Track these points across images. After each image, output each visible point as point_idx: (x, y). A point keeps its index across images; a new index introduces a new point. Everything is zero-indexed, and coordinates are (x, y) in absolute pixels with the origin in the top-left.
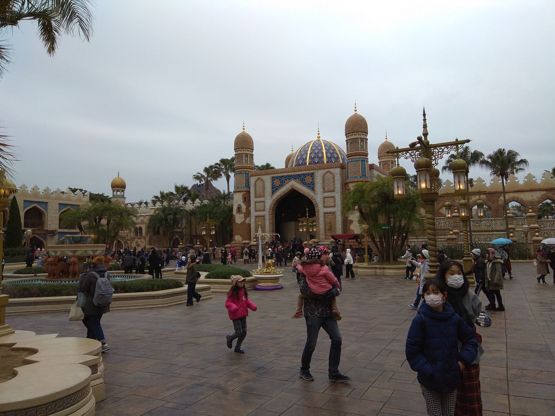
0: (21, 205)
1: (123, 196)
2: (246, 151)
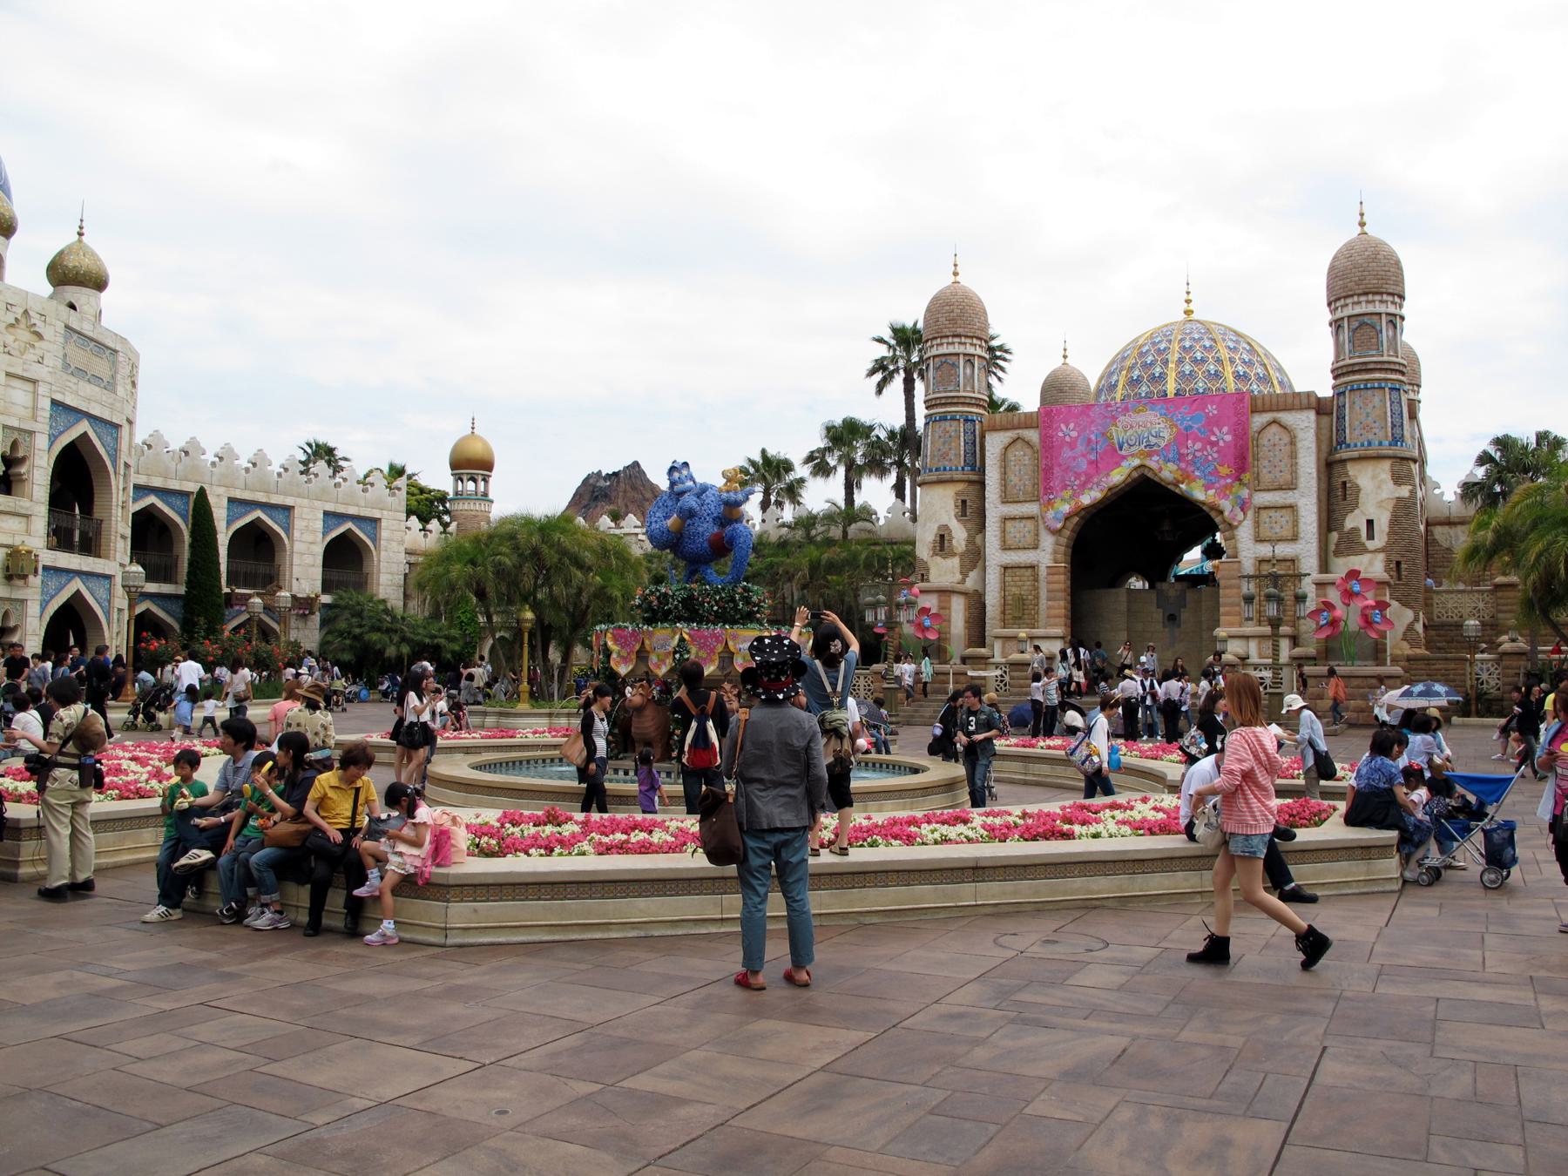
0: (220, 513)
1: (485, 494)
2: (956, 345)
